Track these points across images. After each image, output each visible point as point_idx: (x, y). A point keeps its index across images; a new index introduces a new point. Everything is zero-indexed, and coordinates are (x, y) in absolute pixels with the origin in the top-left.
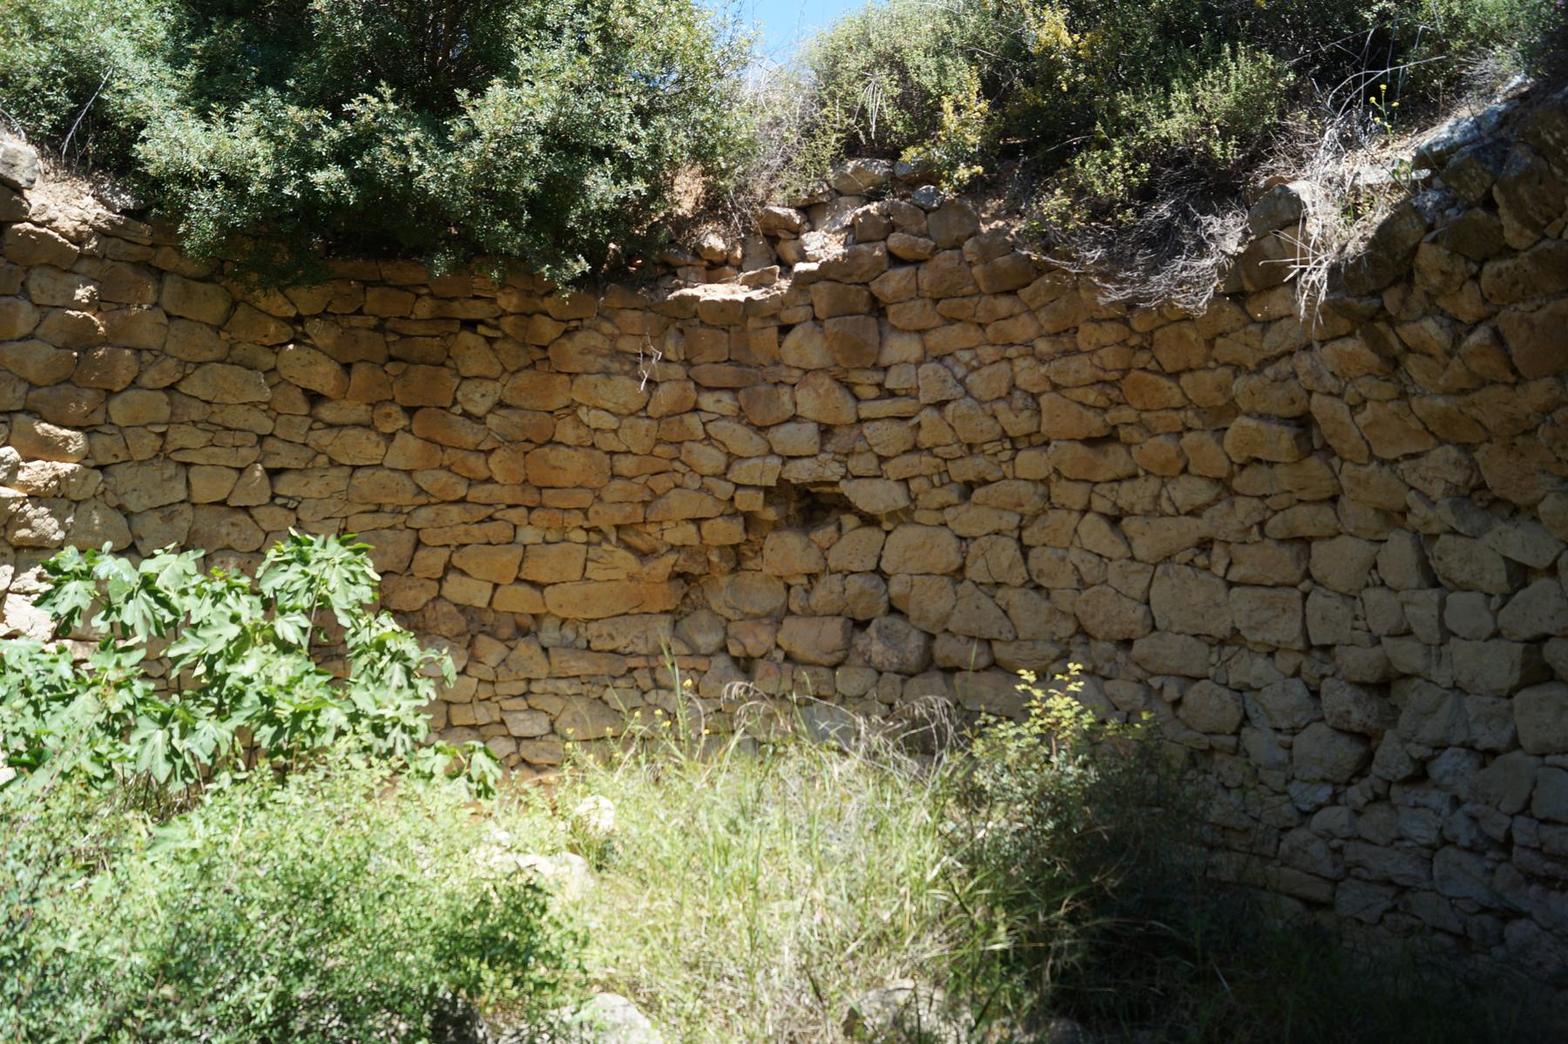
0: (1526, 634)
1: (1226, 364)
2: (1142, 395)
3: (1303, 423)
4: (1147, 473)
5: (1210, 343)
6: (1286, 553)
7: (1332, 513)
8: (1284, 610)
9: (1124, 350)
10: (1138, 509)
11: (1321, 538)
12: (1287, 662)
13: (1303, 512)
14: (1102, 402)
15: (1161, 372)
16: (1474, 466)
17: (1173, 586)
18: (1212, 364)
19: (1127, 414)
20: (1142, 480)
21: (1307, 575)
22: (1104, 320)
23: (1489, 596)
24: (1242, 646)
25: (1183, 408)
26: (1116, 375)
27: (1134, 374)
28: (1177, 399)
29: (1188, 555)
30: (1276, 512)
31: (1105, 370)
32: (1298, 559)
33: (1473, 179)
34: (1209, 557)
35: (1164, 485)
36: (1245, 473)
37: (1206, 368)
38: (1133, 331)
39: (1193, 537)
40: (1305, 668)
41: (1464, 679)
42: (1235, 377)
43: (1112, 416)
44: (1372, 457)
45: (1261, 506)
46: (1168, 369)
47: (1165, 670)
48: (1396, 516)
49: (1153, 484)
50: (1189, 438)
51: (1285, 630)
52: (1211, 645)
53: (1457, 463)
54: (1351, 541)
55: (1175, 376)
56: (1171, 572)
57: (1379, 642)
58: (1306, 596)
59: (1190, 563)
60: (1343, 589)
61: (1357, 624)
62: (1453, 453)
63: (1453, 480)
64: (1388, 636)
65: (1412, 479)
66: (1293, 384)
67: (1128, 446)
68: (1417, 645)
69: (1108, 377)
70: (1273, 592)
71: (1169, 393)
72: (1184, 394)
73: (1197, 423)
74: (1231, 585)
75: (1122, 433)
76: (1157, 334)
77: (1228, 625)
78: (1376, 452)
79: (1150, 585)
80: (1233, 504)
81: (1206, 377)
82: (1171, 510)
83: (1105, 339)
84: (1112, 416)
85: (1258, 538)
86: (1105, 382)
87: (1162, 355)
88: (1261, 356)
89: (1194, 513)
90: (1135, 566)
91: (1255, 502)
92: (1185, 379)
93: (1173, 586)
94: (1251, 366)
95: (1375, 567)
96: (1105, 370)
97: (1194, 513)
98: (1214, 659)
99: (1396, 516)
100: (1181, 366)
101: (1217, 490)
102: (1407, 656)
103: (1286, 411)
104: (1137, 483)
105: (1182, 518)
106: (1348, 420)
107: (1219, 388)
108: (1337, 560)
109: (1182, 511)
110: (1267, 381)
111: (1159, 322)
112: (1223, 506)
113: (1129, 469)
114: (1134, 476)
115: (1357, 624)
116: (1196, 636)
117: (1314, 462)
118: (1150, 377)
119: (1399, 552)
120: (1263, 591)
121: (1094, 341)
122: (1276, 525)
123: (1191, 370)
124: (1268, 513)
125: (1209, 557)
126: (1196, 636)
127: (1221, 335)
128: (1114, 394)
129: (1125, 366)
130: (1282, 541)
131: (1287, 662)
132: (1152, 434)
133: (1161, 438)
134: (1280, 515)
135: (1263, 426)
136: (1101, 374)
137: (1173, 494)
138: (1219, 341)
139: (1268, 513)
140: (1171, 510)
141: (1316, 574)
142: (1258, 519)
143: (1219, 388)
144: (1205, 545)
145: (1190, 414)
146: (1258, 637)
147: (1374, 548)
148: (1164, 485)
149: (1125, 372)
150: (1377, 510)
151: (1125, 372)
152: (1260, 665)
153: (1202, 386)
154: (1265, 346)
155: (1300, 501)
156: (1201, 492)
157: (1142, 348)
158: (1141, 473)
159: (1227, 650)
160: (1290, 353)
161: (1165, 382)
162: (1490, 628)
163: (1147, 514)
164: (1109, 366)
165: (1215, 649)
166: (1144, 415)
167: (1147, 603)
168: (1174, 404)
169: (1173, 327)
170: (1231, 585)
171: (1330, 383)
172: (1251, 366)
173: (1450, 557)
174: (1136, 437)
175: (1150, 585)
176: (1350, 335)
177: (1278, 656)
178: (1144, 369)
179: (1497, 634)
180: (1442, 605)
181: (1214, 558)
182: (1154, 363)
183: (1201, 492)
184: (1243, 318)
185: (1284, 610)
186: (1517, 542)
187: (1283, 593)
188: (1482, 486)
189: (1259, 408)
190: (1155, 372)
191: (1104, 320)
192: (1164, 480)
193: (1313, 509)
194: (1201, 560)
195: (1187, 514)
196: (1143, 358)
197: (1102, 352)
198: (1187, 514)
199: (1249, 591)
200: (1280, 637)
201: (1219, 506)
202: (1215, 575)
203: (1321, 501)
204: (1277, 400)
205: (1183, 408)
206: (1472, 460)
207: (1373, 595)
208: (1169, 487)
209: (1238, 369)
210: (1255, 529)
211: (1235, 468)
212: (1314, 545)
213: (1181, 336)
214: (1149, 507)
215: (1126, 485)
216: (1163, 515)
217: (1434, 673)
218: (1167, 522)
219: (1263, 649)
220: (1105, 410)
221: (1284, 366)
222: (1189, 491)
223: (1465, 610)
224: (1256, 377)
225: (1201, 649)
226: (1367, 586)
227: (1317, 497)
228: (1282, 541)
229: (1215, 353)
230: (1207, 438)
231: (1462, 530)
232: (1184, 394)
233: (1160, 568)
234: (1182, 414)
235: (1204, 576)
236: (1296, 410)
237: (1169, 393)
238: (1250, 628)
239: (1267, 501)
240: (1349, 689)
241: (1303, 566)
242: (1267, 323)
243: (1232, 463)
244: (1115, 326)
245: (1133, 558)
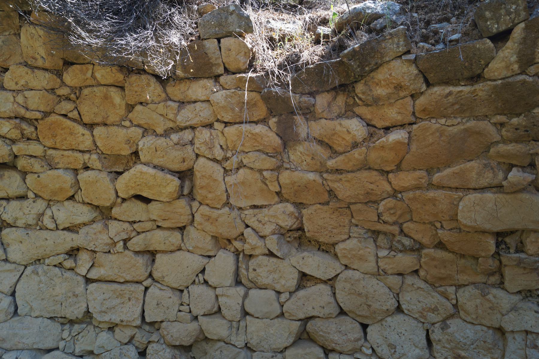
0: (302, 316)
1: (139, 126)
2: (54, 136)
3: (185, 175)
4: (36, 196)
5: (130, 108)
6: (141, 261)
7: (180, 236)
8: (129, 299)
9: (51, 96)
10: (20, 223)
11: (164, 252)
12: (123, 335)
13: (159, 234)
14: (15, 134)
15: (80, 121)
16: (300, 218)
17: (40, 282)
18: (127, 123)
19: (35, 149)
20: (30, 201)
21: (150, 275)
22: (36, 68)
23: (279, 293)
24: (90, 323)
25: (89, 151)
26: (38, 115)
27: (53, 118)
28: (87, 144)
29: (61, 258)
30: (139, 233)
31: (27, 109)
32: (147, 266)
33: (509, 13)
34: (75, 261)
35: (49, 206)
36: (125, 205)
37: (120, 125)
38: (63, 84)
39: (68, 247)
40: (138, 337)
41: (253, 342)
42: (143, 136)
43: (19, 148)
44: (227, 203)
45: (130, 228)
46: (86, 120)
47: (20, 346)
48: (221, 242)
49: (40, 205)
50: (84, 176)
51: (130, 312)
52: (63, 324)
53: (291, 214)
54: (188, 255)
55: (91, 126)
56: (40, 271)
57: (196, 318)
58: (147, 289)
59: (60, 265)
60: (175, 285)
61: (182, 308)
62: (290, 208)
63: (283, 224)
64: (204, 315)
65: (251, 222)
66: (189, 148)
67: (24, 174)
68: (225, 321)
69: (28, 115)
70: (123, 287)
71: (81, 139)
72: (94, 142)
73: (98, 165)
74: (88, 281)
75: (21, 163)
76: (86, 91)
77: (83, 309)
78: (231, 201)
79: (18, 281)
80: (106, 226)
81: (121, 134)
82: (52, 226)
83: (33, 84)
84: (19, 148)
85: (121, 250)
86: (23, 119)
87: (84, 109)
88: (171, 125)
89: (71, 229)
90: (8, 266)
91: (127, 225)
92: (98, 131)
93: (40, 282)
94: (160, 131)
95: (203, 271)
96: (27, 109)
97: (71, 229)
98: (65, 334)
99: (221, 242)
100: (98, 120)
101: (95, 215)
102: (216, 327)
103: (176, 167)
104: (25, 203)
105: (61, 232)
106: (221, 179)
107: (128, 142)
108: (174, 268)
109: (61, 227)
110: (171, 143)
111: (89, 82)
112: (98, 226)
113: (21, 191)
114: (22, 197)
115: (182, 308)
116: (51, 318)
117: (182, 203)
118: (69, 123)
119: (223, 264)
120: (115, 286)
121: (22, 82)
122: (137, 243)
123: (105, 125)
124: (134, 234)
125: (75, 261)
126: (51, 318)
127: (141, 103)
128: (29, 130)
129: (48, 109)
130: (137, 253)
131: (123, 335)
132: (52, 167)
133: (61, 172)
134: (142, 236)
135: (160, 174)
136: (22, 111)
137: (56, 213)
138: (139, 108)
139: (134, 234)
140: (52, 226)
141: (156, 275)
142: (125, 237)
143: (128, 142)
144: (73, 253)
145: (94, 157)
146: (107, 319)
147: (206, 260)
148: (49, 206)
149: (46, 114)
150: (212, 236)
151: (46, 114)
152: (104, 337)
153: (114, 139)
154: (179, 118)
155: (158, 227)
156: (83, 214)
157: (68, 99)
158: (31, 195)
159: (76, 327)
160: (193, 128)
161: (80, 129)
162: (279, 312)
163: (28, 227)
164: (32, 106)
165: (67, 327)
166: (50, 152)
167: (13, 294)
168: (82, 147)
169: (101, 88)
170: (88, 281)
171: (218, 153)
172: (160, 131)
173: (262, 269)
174: (37, 167)
175: (18, 281)
176: (264, 121)
177: (117, 330)
178: (65, 116)
179: (282, 315)
180: (246, 296)
181: (80, 263)
182: (75, 112)
183: (81, 214)
184: (164, 95)
185: (129, 299)
186: (314, 263)
187: (132, 287)
188: (301, 229)
189: (156, 161)
190: (74, 120)
191: (36, 68)
192: (49, 203)
193: (167, 233)
194: (69, 263)
195: (64, 229)
196: (66, 107)
197: (28, 94)
198: (64, 229)
199: (104, 286)
200: (123, 318)
201: (94, 226)
202: (78, 274)
203: (116, 219)
204: (174, 159)
205: (89, 151)
206: (300, 213)
207: (197, 290)
208: (54, 208)
209: (146, 131)
210: (121, 243)
211: (119, 200)
212: (158, 256)
213: (106, 97)
214: (31, 221)
215: (14, 204)
216: (44, 228)
217: (233, 339)
218: (45, 234)
219: (106, 326)
220: (13, 141)
221: (187, 135)
222: (66, 213)
223: (258, 300)
224: (163, 139)
225: (56, 327)
226: (194, 282)
227: (174, 226)
228: (137, 253)
229: (130, 115)
230: (104, 178)
231: (279, 255)
232: (94, 142)
233: (30, 269)
234: (87, 156)
235: (69, 274)
236: (184, 167)
237: (81, 139)
238: (101, 312)
239: (135, 226)
240: (168, 350)
241: (149, 271)
242: (182, 103)
243: (118, 196)
244: (47, 75)
245: (6, 260)
